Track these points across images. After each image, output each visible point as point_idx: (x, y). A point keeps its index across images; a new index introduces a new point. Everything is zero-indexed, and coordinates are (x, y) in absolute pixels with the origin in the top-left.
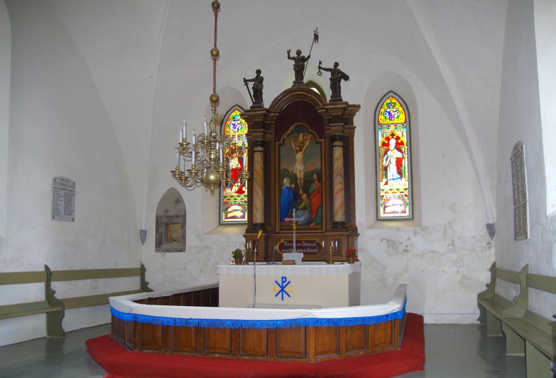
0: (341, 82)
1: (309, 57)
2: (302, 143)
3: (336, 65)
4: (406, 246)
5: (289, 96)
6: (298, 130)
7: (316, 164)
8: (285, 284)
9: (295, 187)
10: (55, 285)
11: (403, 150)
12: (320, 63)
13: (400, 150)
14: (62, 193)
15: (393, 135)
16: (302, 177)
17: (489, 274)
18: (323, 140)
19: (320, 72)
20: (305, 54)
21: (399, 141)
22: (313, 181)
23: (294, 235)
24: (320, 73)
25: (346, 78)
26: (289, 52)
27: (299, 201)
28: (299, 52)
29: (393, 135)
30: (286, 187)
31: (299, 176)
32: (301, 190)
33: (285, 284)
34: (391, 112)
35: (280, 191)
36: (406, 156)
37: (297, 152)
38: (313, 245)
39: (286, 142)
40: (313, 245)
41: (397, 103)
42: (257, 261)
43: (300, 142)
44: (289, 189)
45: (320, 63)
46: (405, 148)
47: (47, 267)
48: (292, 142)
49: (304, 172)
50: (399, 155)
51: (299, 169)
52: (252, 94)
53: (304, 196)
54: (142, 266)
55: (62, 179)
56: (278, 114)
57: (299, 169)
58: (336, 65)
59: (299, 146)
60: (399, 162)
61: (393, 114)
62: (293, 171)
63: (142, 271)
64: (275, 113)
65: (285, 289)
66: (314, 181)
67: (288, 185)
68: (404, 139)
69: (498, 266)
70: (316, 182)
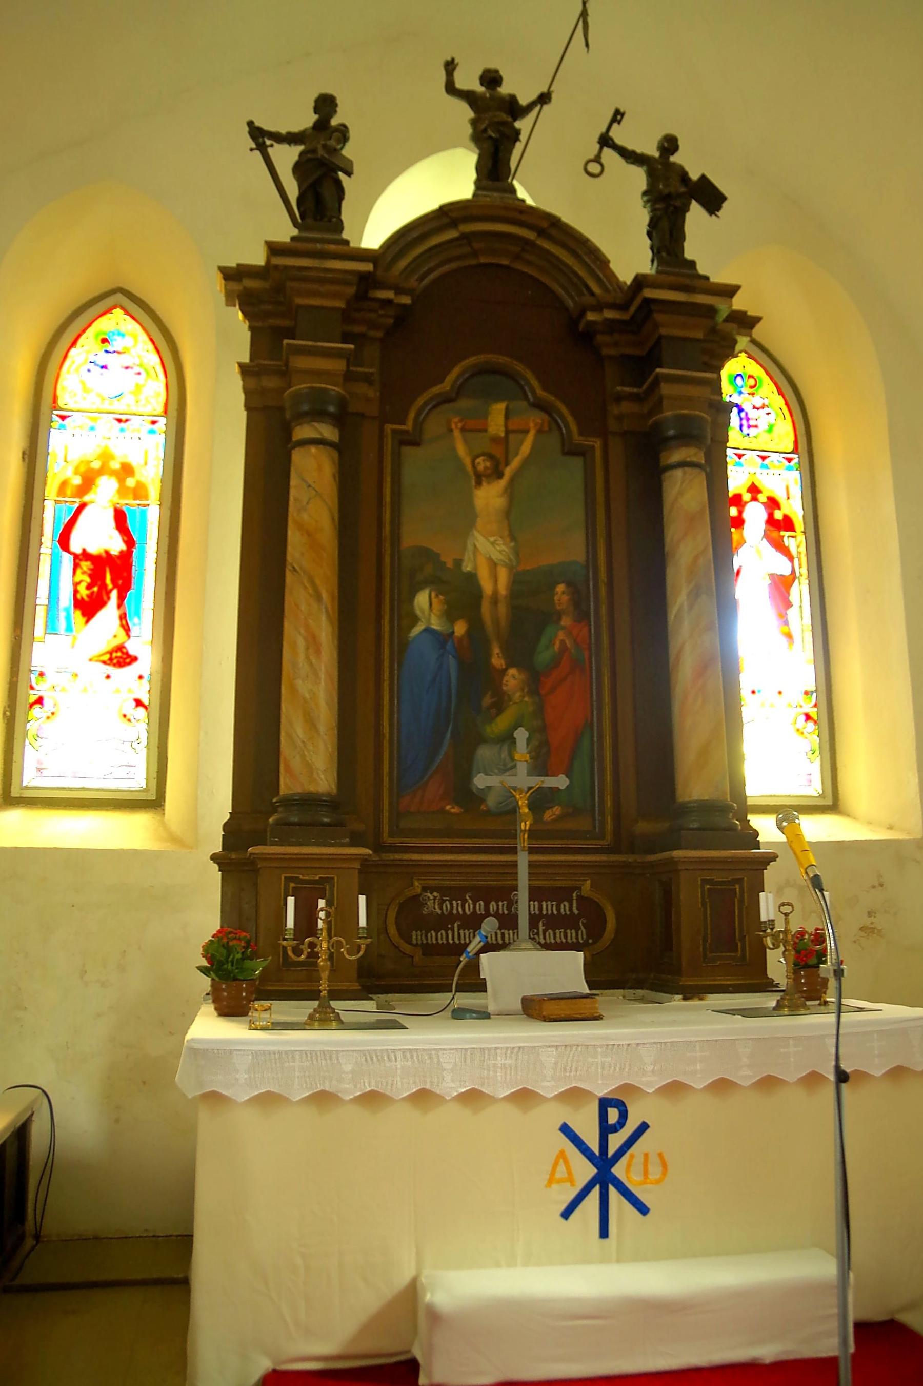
0: (688, 216)
1: (544, 98)
2: (504, 442)
3: (670, 145)
4: (870, 914)
5: (452, 234)
6: (490, 382)
7: (566, 543)
8: (615, 1141)
9: (468, 633)
11: (794, 552)
12: (617, 116)
15: (754, 490)
16: (503, 590)
19: (597, 159)
20: (519, 86)
21: (778, 515)
22: (550, 617)
23: (523, 860)
24: (594, 168)
25: (713, 200)
26: (450, 66)
27: (487, 701)
28: (491, 79)
30: (428, 630)
31: (487, 586)
32: (496, 650)
33: (615, 1141)
34: (747, 407)
35: (402, 646)
36: (804, 571)
37: (479, 479)
38: (565, 908)
39: (433, 427)
40: (565, 908)
41: (766, 379)
42: (336, 995)
43: (495, 440)
44: (441, 639)
45: (617, 116)
46: (796, 542)
48: (457, 434)
49: (511, 568)
50: (782, 566)
51: (488, 557)
52: (293, 192)
53: (513, 679)
56: (406, 300)
57: (488, 557)
58: (670, 145)
59: (491, 457)
60: (781, 587)
61: (752, 414)
62: (458, 563)
64: (399, 291)
66: (559, 615)
67: (436, 624)
68: (793, 507)
70: (566, 621)
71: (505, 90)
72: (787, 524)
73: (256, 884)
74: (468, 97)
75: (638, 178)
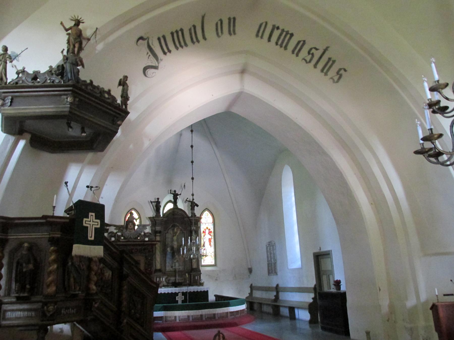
1: (180, 194)
13: (210, 235)
15: (207, 228)
17: (250, 289)
18: (185, 232)
25: (197, 206)
28: (175, 191)
29: (207, 228)
46: (212, 234)
50: (210, 237)
60: (210, 240)
69: (253, 285)
71: (176, 192)
72: (211, 232)
73: (438, 300)
74: (173, 194)
75: (190, 203)
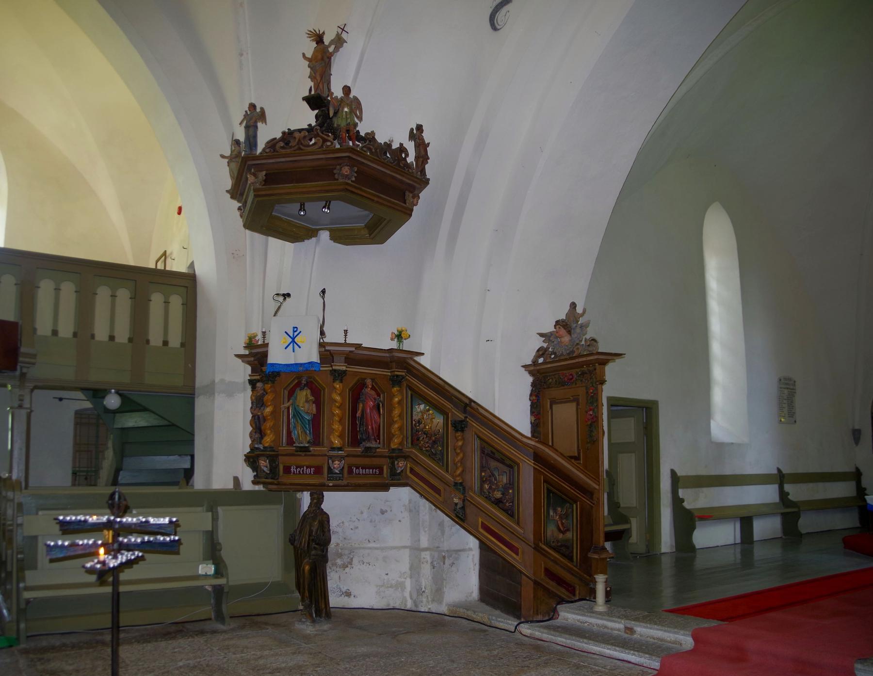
8: (296, 334)
10: (787, 487)
14: (786, 391)
33: (296, 334)
47: (779, 470)
54: (858, 470)
55: (785, 379)
63: (857, 475)
65: (296, 340)
